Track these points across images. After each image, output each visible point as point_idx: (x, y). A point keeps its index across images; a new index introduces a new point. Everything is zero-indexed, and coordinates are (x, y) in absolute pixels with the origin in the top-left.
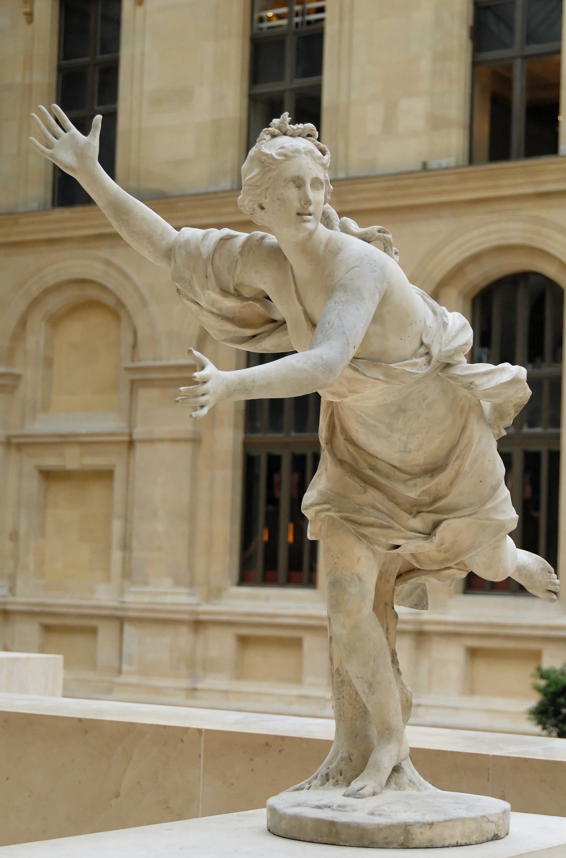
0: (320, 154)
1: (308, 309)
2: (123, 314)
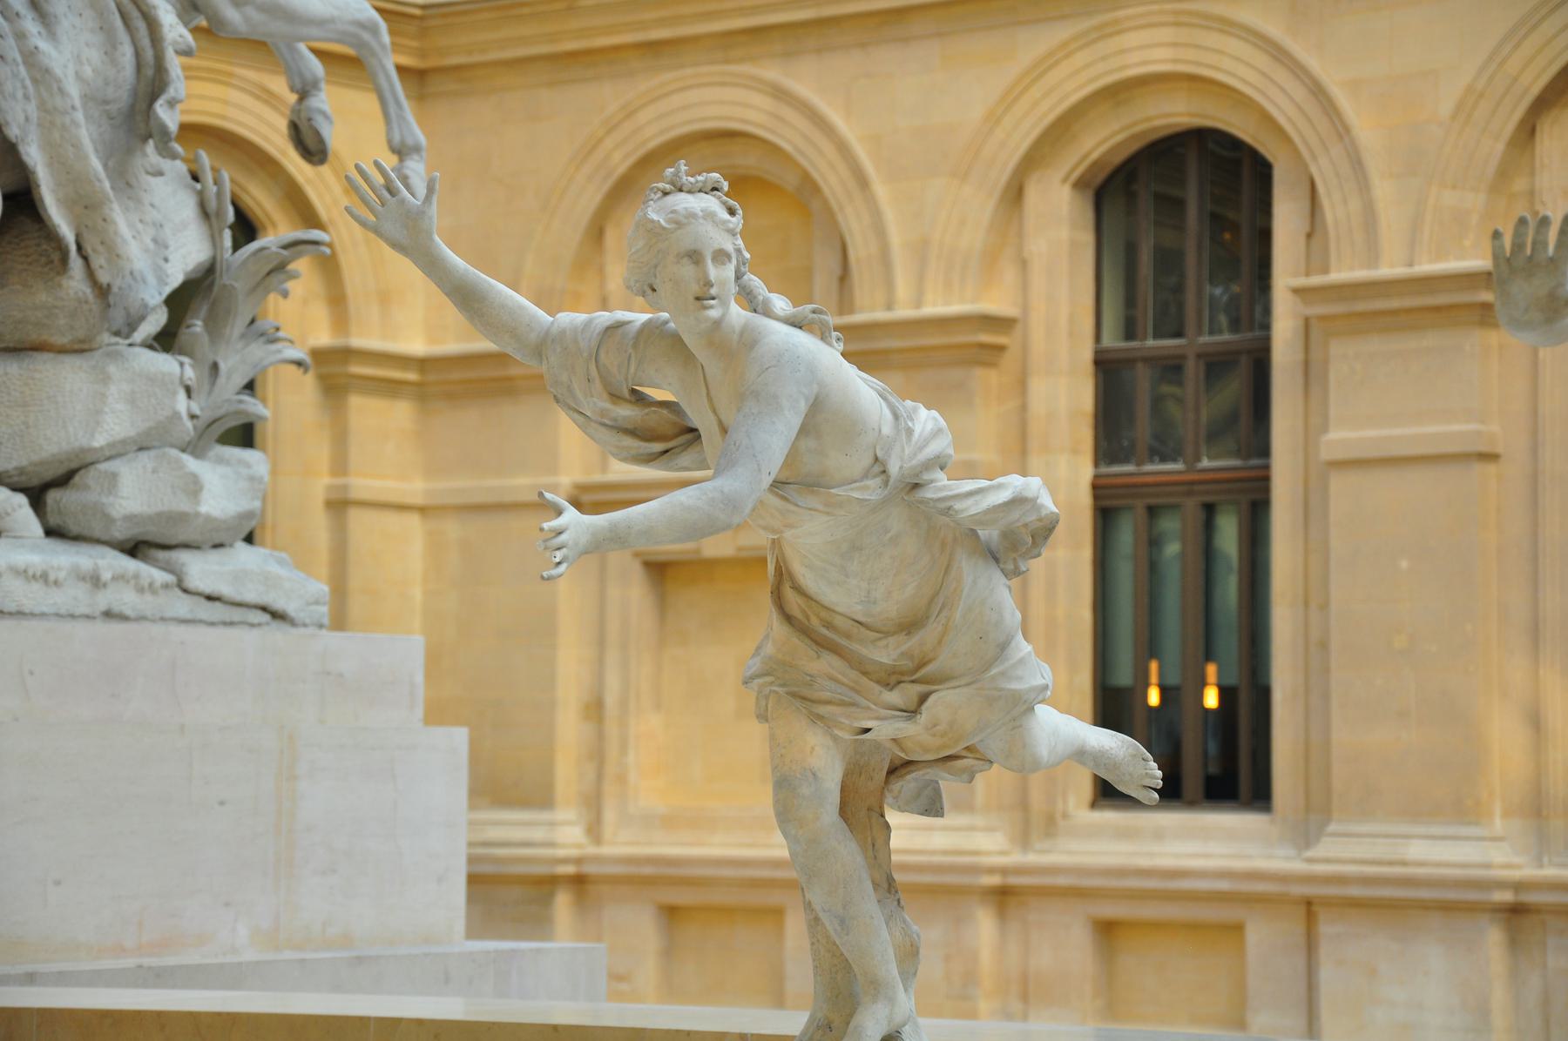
0: (727, 216)
1: (723, 418)
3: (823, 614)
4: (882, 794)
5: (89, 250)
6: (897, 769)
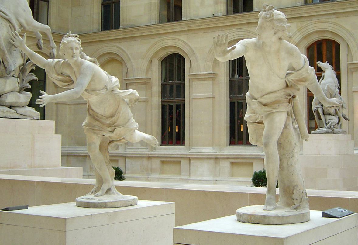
0: (78, 41)
2: (123, 63)
3: (96, 114)
4: (108, 146)
5: (4, 62)
6: (111, 142)
